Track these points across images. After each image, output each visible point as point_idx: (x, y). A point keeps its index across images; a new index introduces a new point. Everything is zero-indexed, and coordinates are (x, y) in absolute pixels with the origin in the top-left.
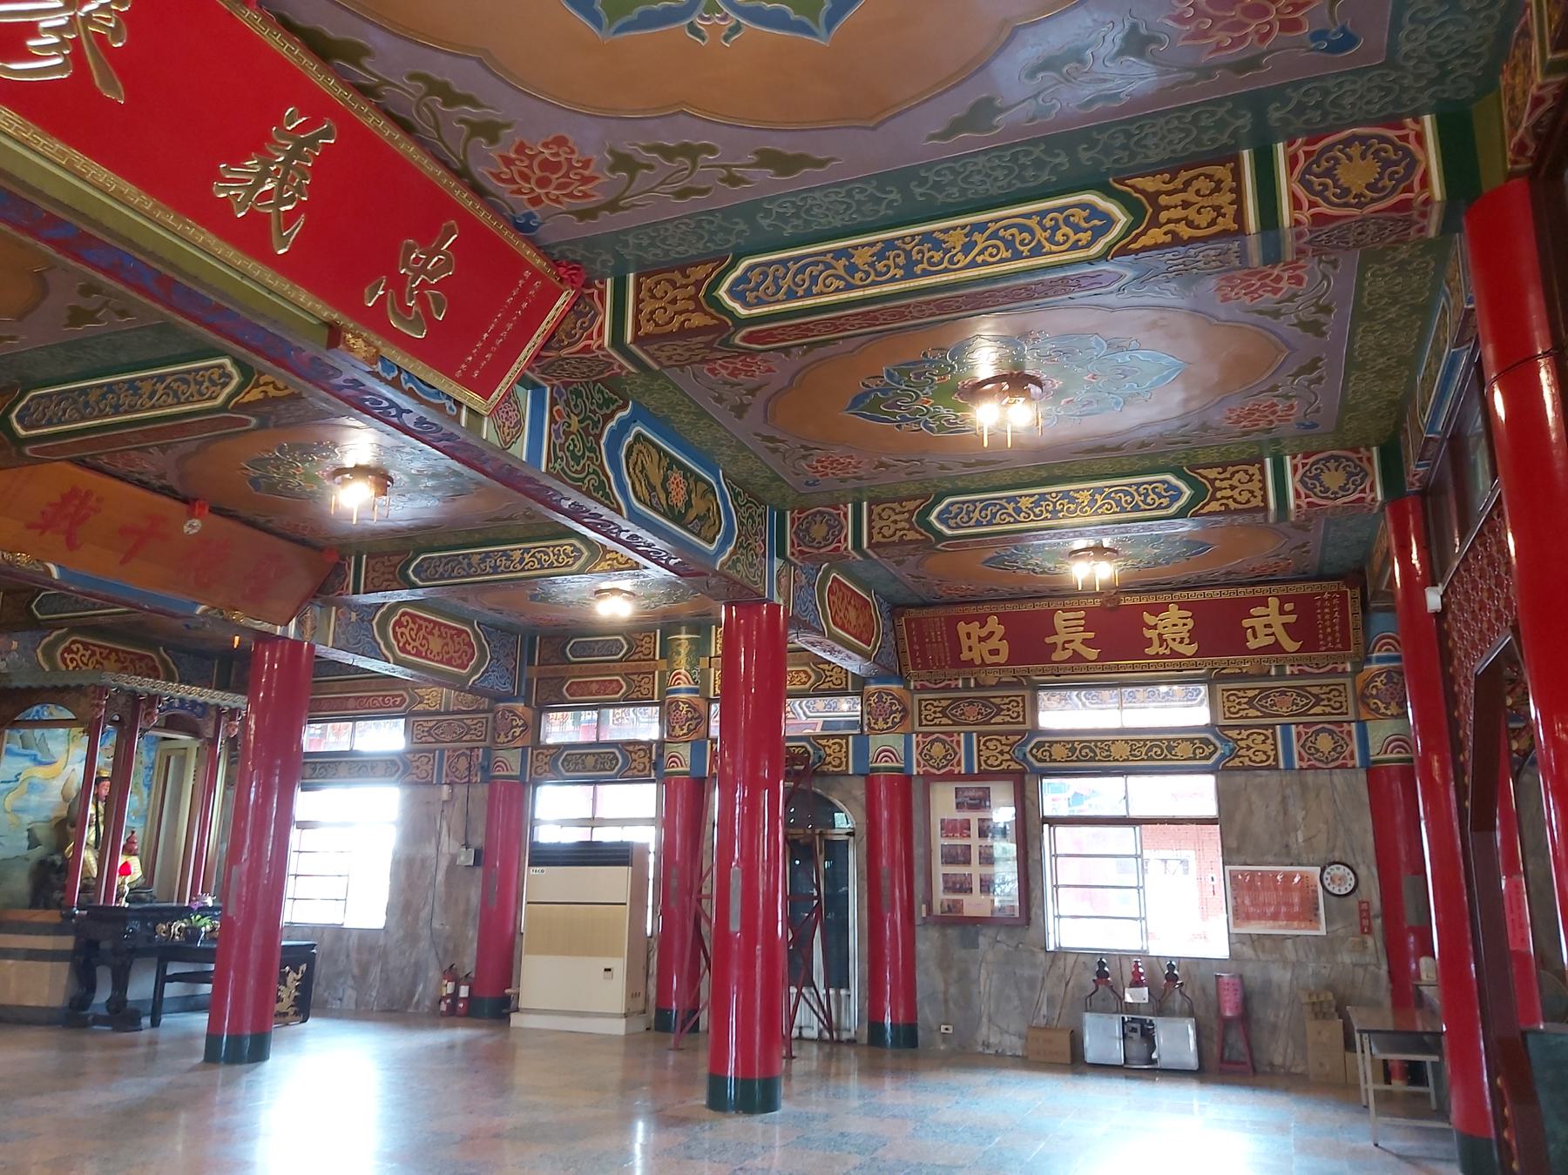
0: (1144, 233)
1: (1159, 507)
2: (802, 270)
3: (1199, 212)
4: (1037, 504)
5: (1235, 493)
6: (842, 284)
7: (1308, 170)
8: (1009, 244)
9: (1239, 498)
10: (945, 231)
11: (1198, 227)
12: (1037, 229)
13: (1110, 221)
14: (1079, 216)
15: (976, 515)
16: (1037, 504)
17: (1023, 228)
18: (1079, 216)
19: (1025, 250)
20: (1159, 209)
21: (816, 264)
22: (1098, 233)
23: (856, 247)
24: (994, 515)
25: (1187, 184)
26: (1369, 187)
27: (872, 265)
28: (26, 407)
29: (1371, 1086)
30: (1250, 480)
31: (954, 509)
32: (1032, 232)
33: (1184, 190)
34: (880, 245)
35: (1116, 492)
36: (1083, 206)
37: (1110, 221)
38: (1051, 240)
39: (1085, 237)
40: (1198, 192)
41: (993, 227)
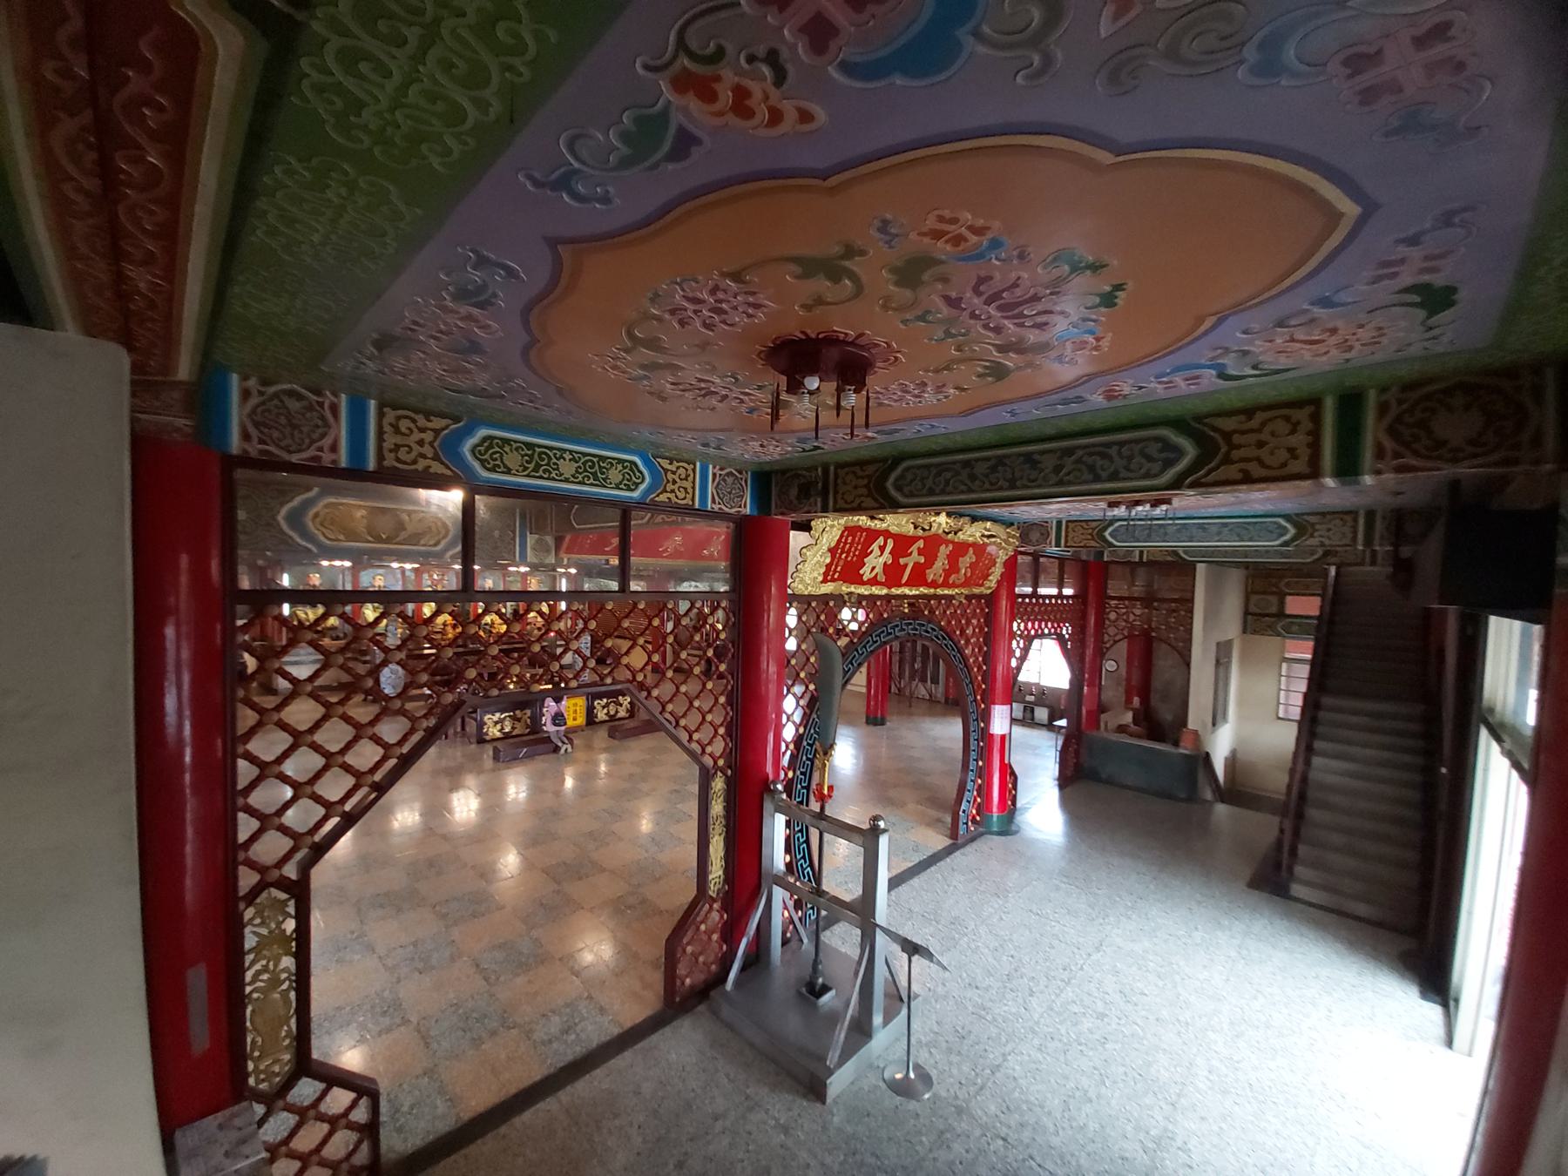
0: (1218, 467)
1: (1147, 476)
2: (939, 474)
3: (1272, 453)
4: (994, 469)
5: (1263, 453)
6: (963, 488)
7: (1398, 419)
8: (1092, 469)
9: (1268, 460)
10: (1043, 452)
11: (1269, 467)
12: (1116, 458)
13: (1179, 452)
14: (1153, 449)
15: (929, 483)
16: (994, 469)
17: (1104, 456)
18: (1153, 449)
19: (1104, 475)
20: (1233, 447)
21: (947, 470)
22: (1168, 464)
23: (977, 460)
24: (947, 482)
25: (1264, 424)
26: (1471, 442)
27: (987, 476)
28: (901, 477)
29: (976, 301)
30: (1293, 432)
31: (909, 476)
32: (1111, 459)
33: (1259, 431)
34: (993, 462)
35: (1090, 454)
36: (1157, 439)
37: (1179, 452)
38: (1128, 469)
39: (1156, 467)
40: (1273, 434)
41: (1080, 453)
